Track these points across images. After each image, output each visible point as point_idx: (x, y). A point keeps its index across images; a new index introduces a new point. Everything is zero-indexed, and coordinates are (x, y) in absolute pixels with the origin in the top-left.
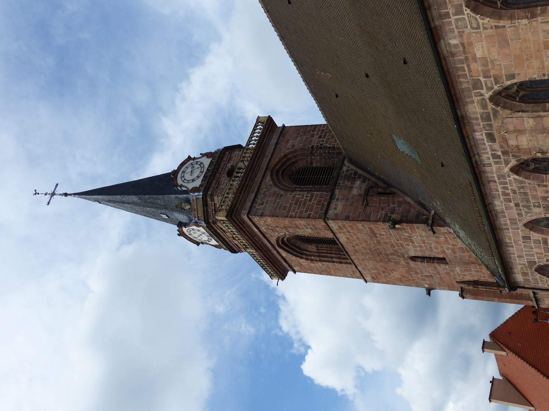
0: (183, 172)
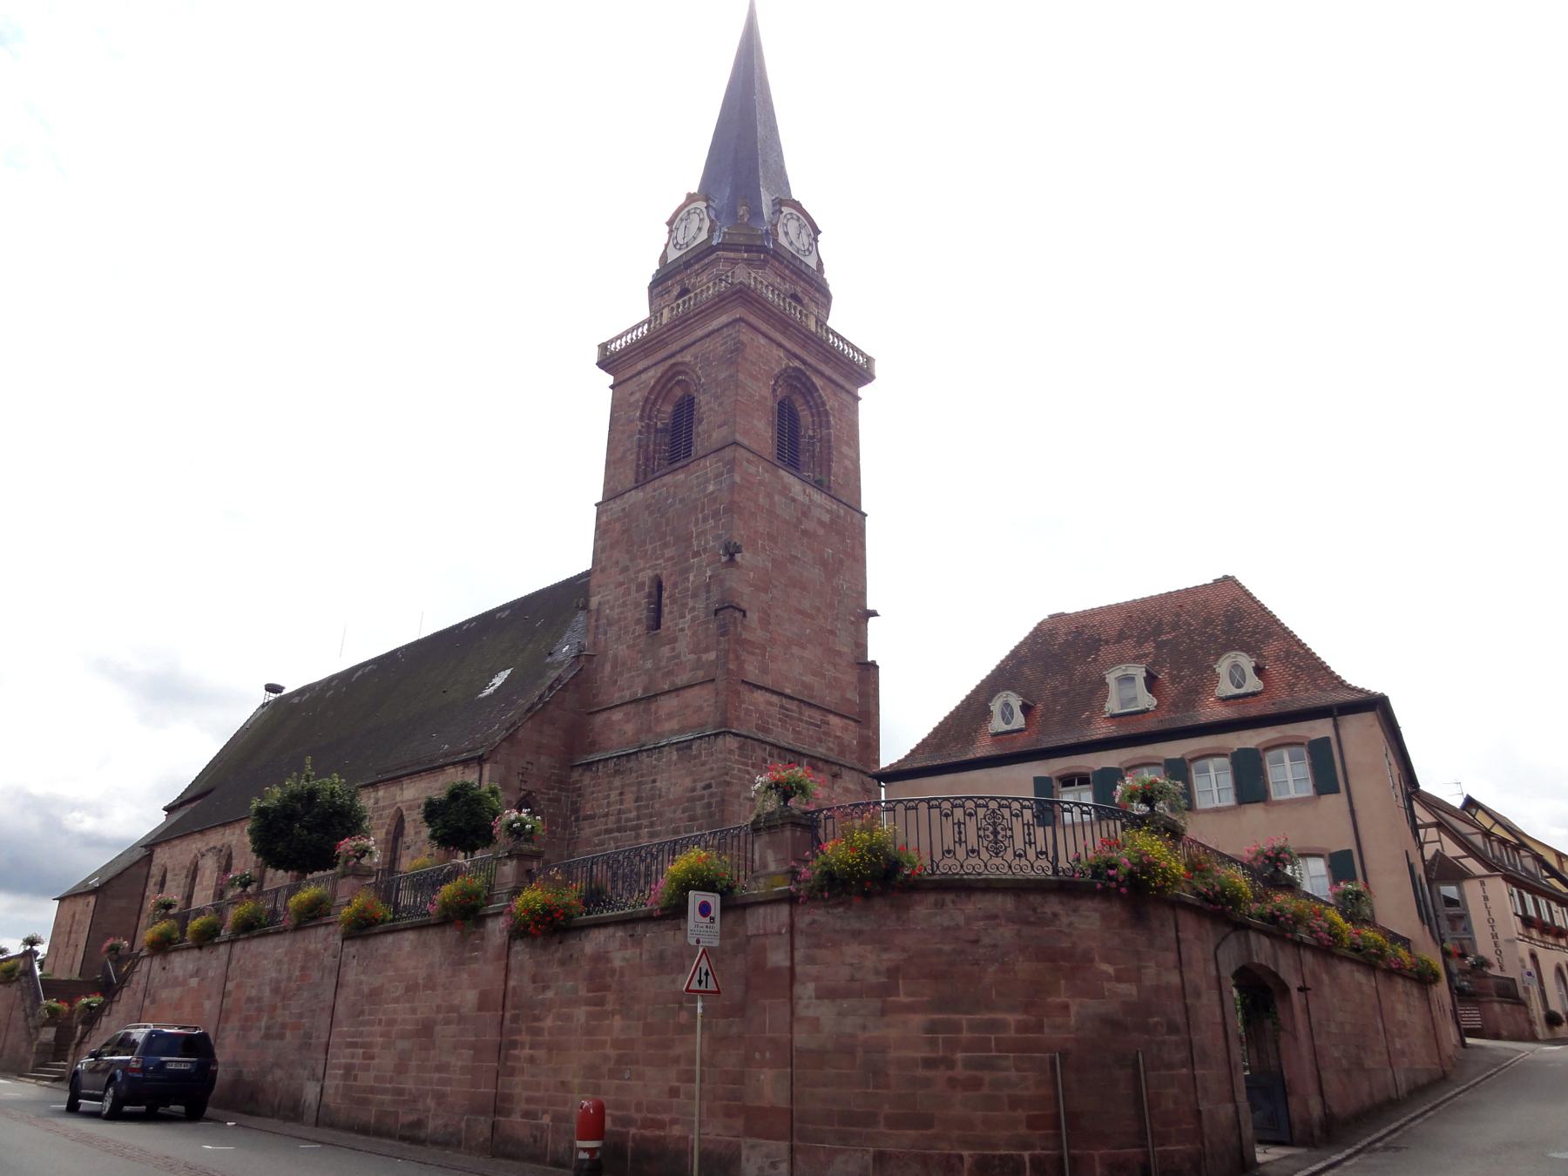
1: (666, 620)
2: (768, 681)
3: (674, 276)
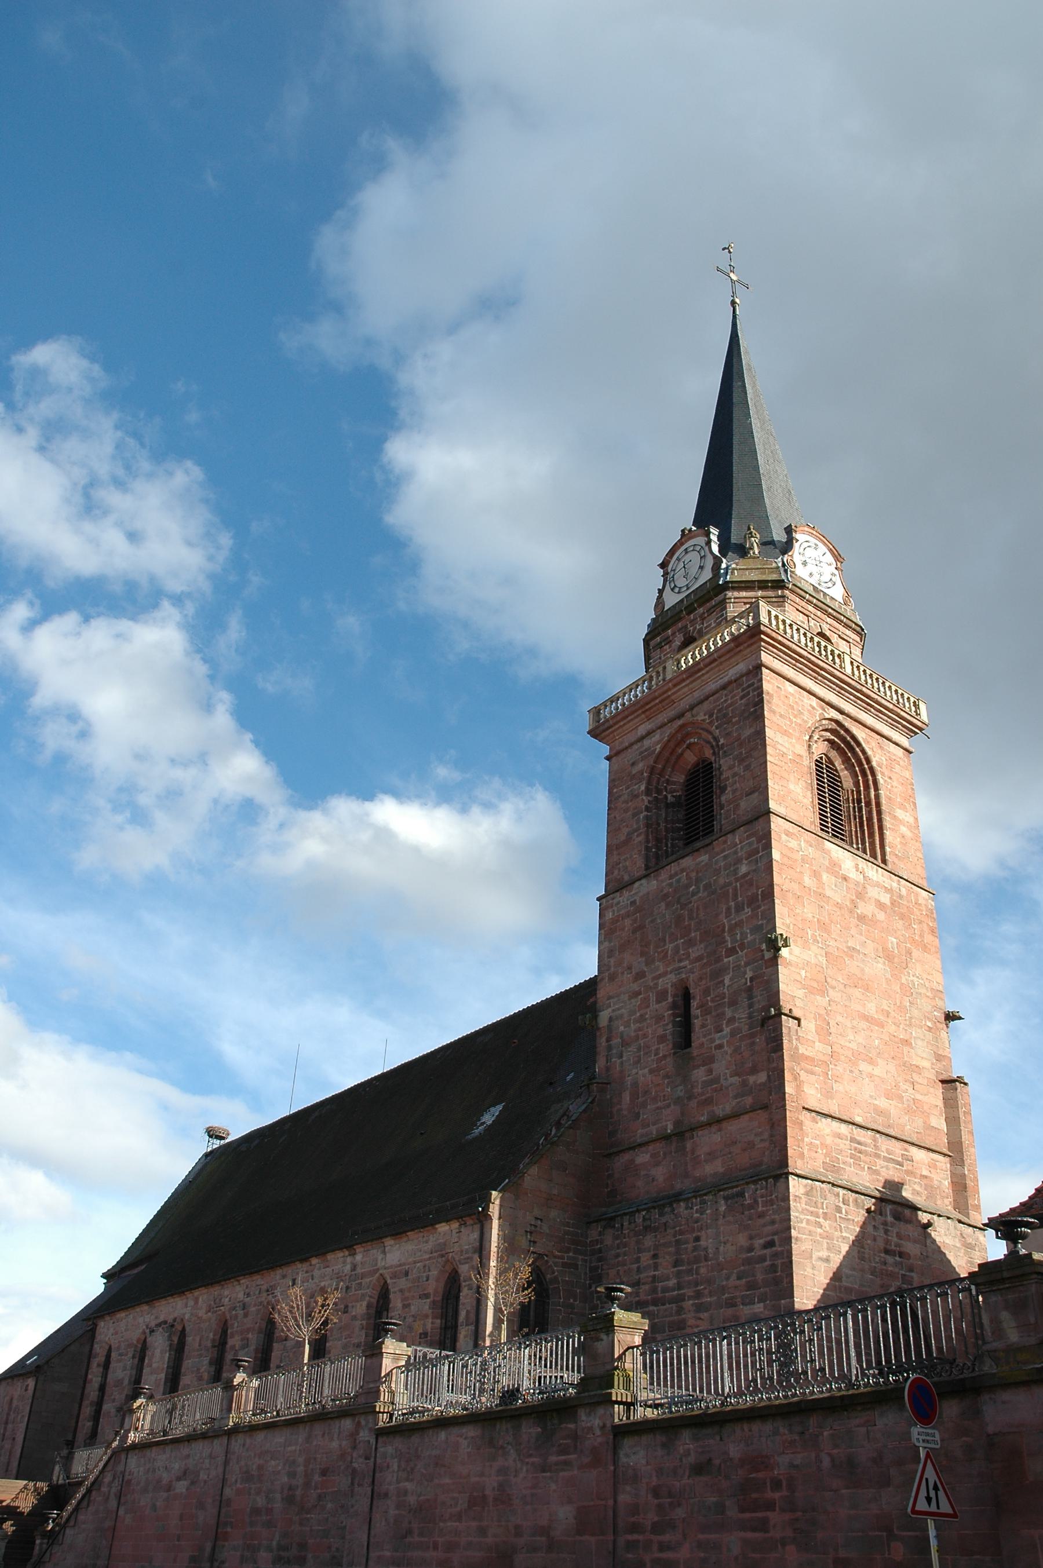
1: (698, 1037)
2: (833, 1108)
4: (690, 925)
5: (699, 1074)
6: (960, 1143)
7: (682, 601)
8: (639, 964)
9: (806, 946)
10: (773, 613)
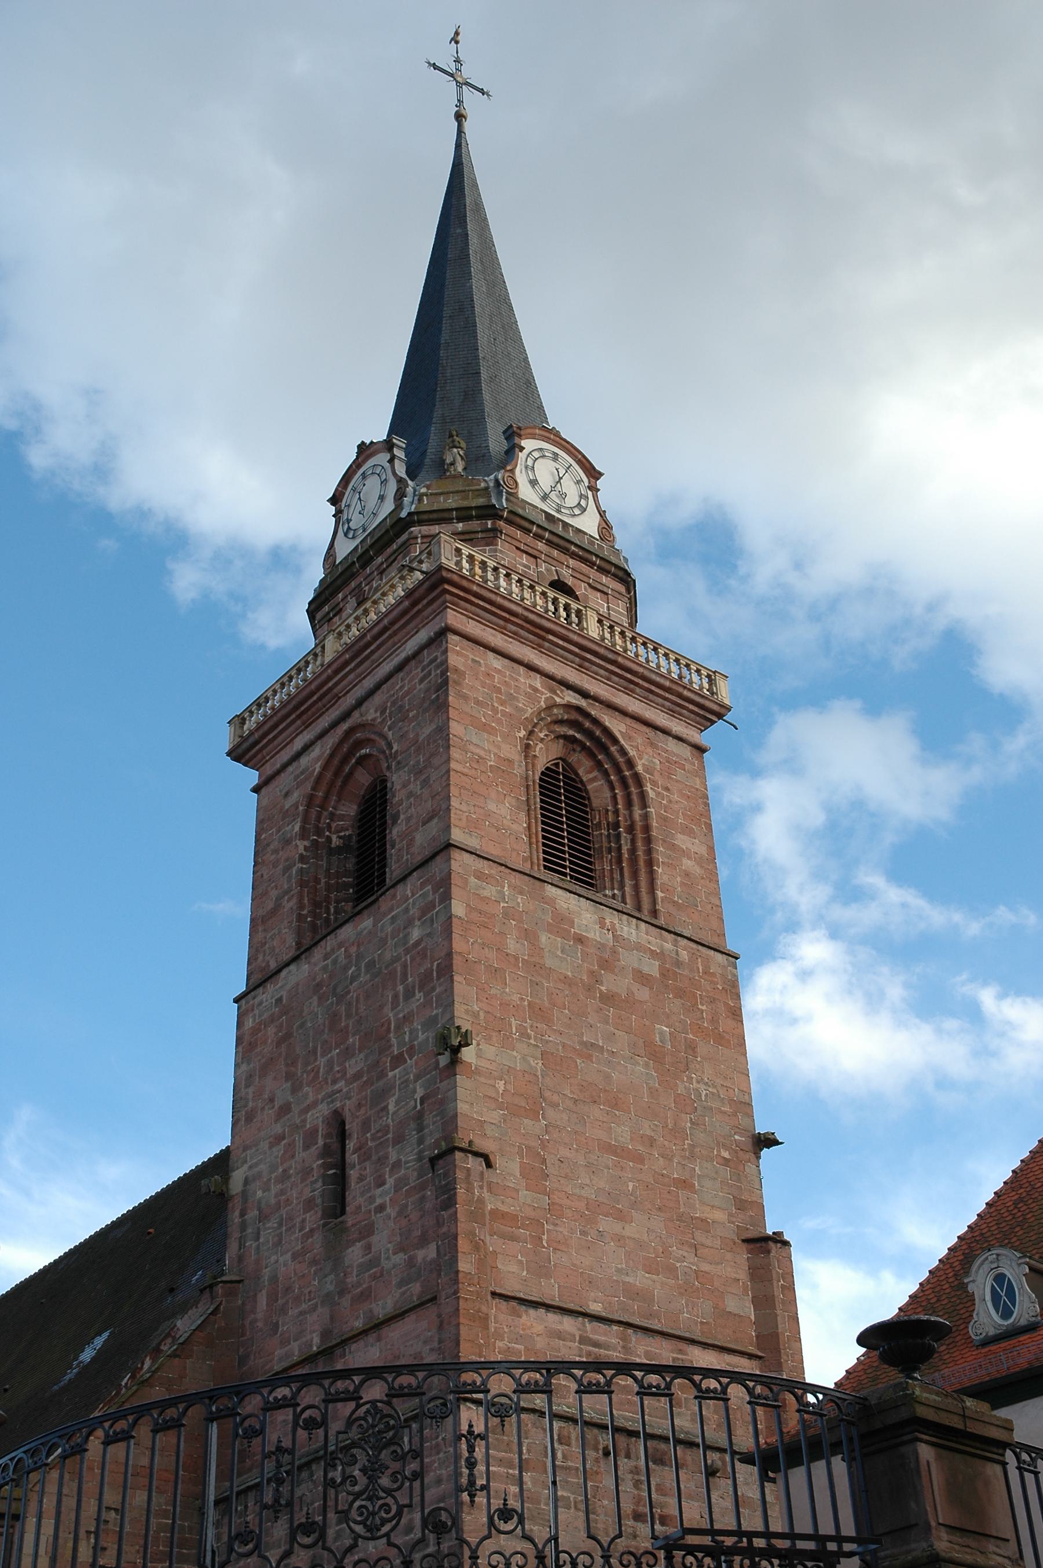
0: (556, 455)
1: (355, 1197)
2: (551, 1291)
3: (346, 583)
4: (347, 1026)
5: (354, 1255)
6: (775, 1336)
7: (356, 548)
8: (283, 1092)
9: (507, 1042)
10: (465, 551)
